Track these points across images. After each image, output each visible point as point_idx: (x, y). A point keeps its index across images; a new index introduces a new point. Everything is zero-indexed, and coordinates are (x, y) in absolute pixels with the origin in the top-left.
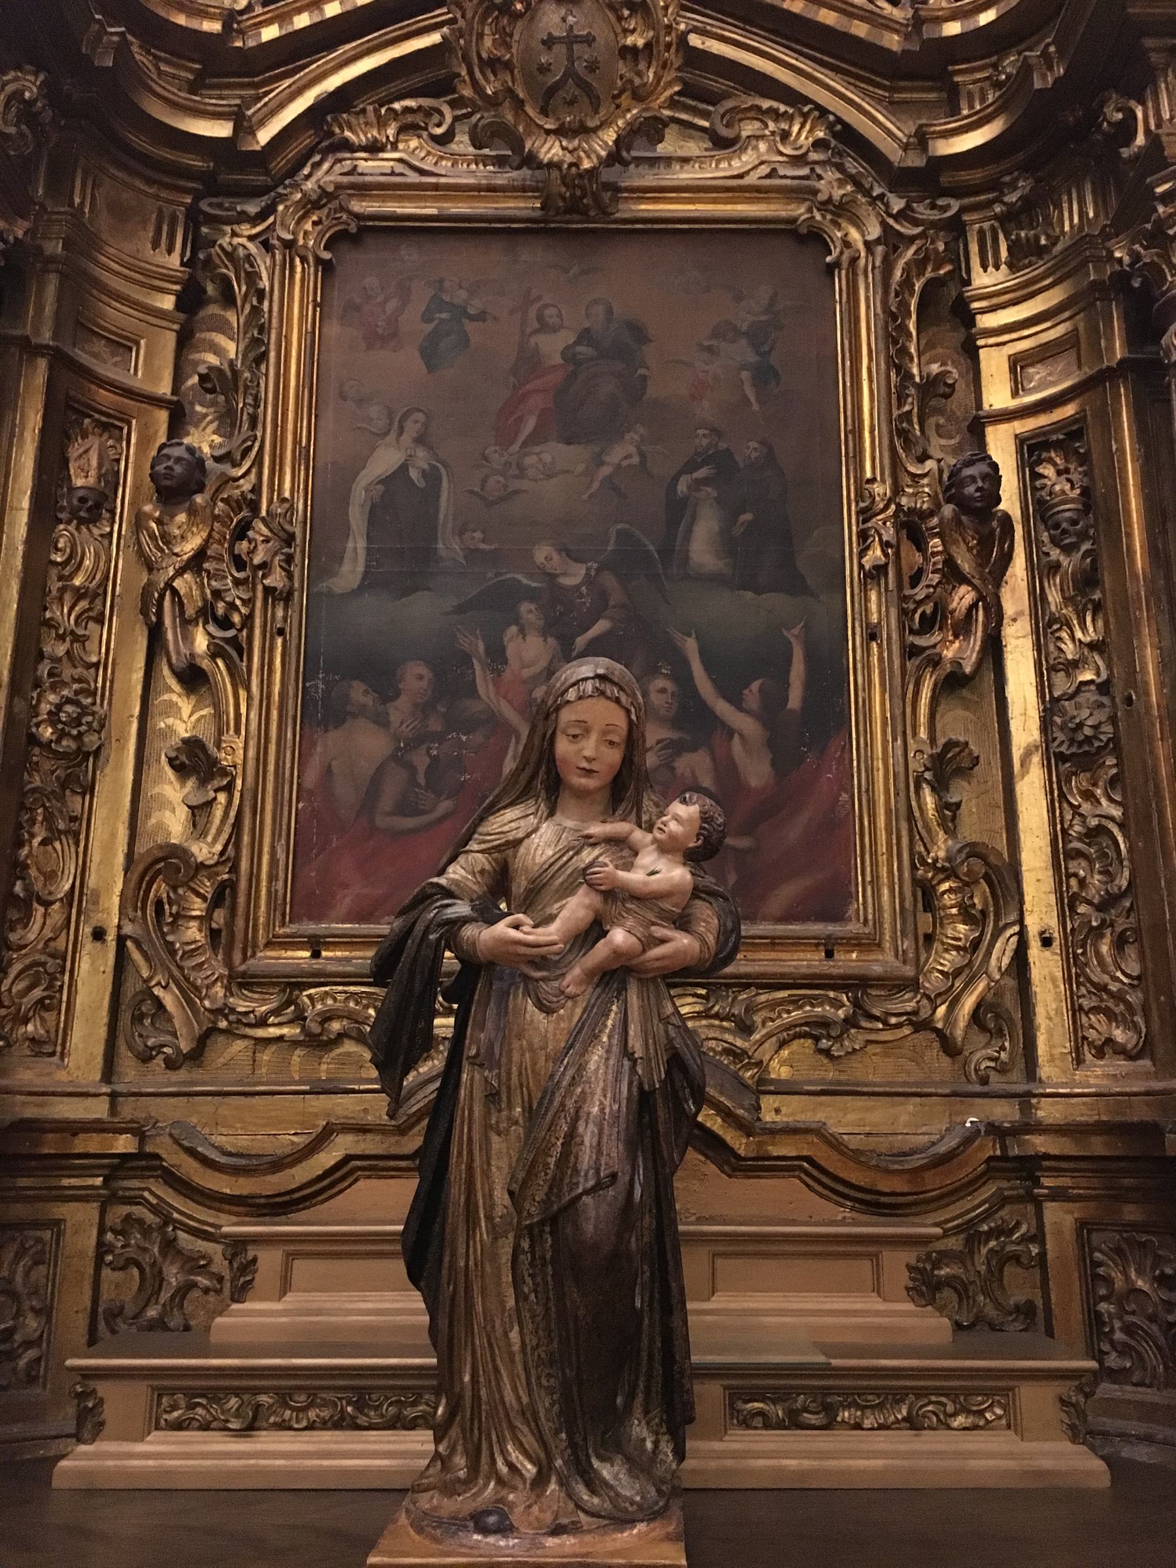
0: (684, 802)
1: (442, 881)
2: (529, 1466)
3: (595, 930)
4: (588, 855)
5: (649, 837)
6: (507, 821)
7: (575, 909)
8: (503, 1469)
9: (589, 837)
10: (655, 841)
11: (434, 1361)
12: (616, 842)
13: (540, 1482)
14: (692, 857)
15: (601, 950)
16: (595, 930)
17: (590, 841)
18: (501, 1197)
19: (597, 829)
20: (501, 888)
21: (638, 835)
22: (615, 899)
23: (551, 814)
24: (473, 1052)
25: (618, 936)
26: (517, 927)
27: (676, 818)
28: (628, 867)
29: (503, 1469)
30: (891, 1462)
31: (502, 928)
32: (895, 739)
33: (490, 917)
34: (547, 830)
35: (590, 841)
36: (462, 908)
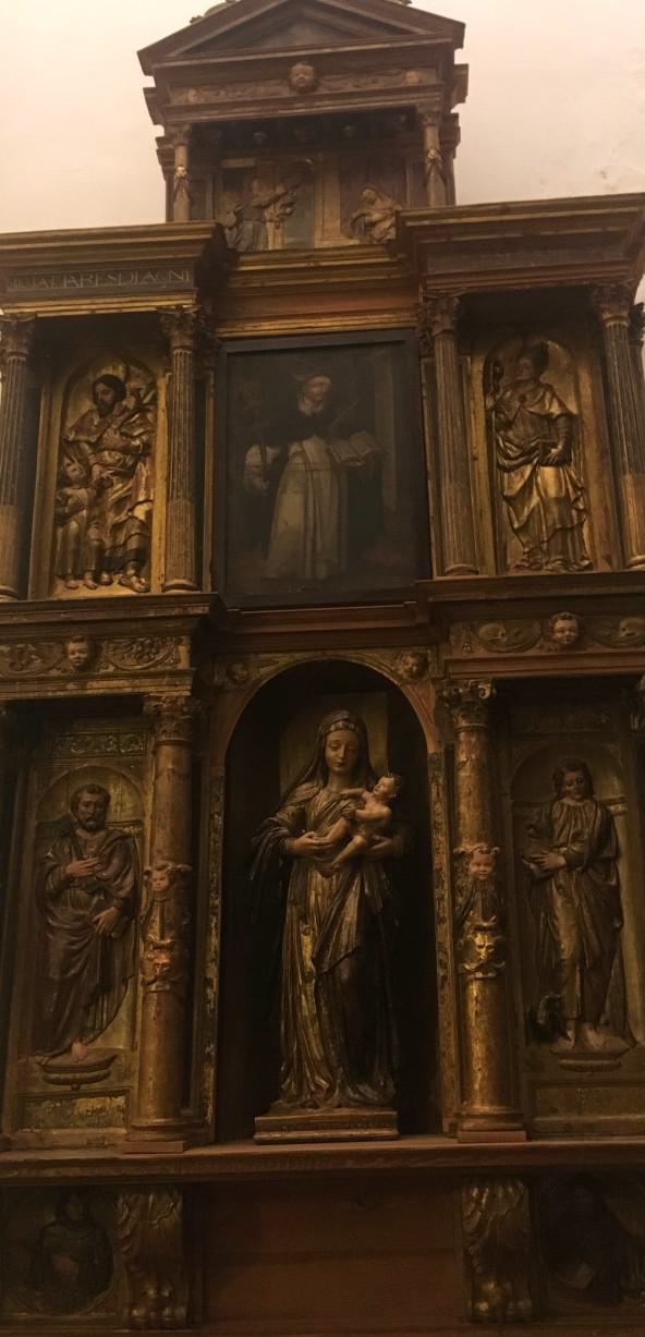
0: (387, 776)
1: (275, 819)
2: (324, 1082)
3: (346, 838)
4: (343, 803)
5: (371, 795)
6: (304, 791)
7: (336, 829)
8: (313, 1088)
9: (342, 795)
10: (374, 796)
11: (256, 1119)
12: (356, 797)
13: (331, 1090)
14: (389, 804)
15: (350, 847)
16: (346, 838)
17: (343, 798)
18: (309, 963)
19: (346, 792)
20: (301, 824)
21: (366, 795)
22: (354, 823)
23: (325, 785)
24: (292, 898)
25: (358, 839)
26: (310, 837)
27: (384, 784)
28: (363, 808)
29: (313, 1088)
30: (298, 656)
31: (304, 839)
32: (108, 846)
33: (298, 835)
34: (323, 794)
35: (343, 798)
36: (285, 831)
